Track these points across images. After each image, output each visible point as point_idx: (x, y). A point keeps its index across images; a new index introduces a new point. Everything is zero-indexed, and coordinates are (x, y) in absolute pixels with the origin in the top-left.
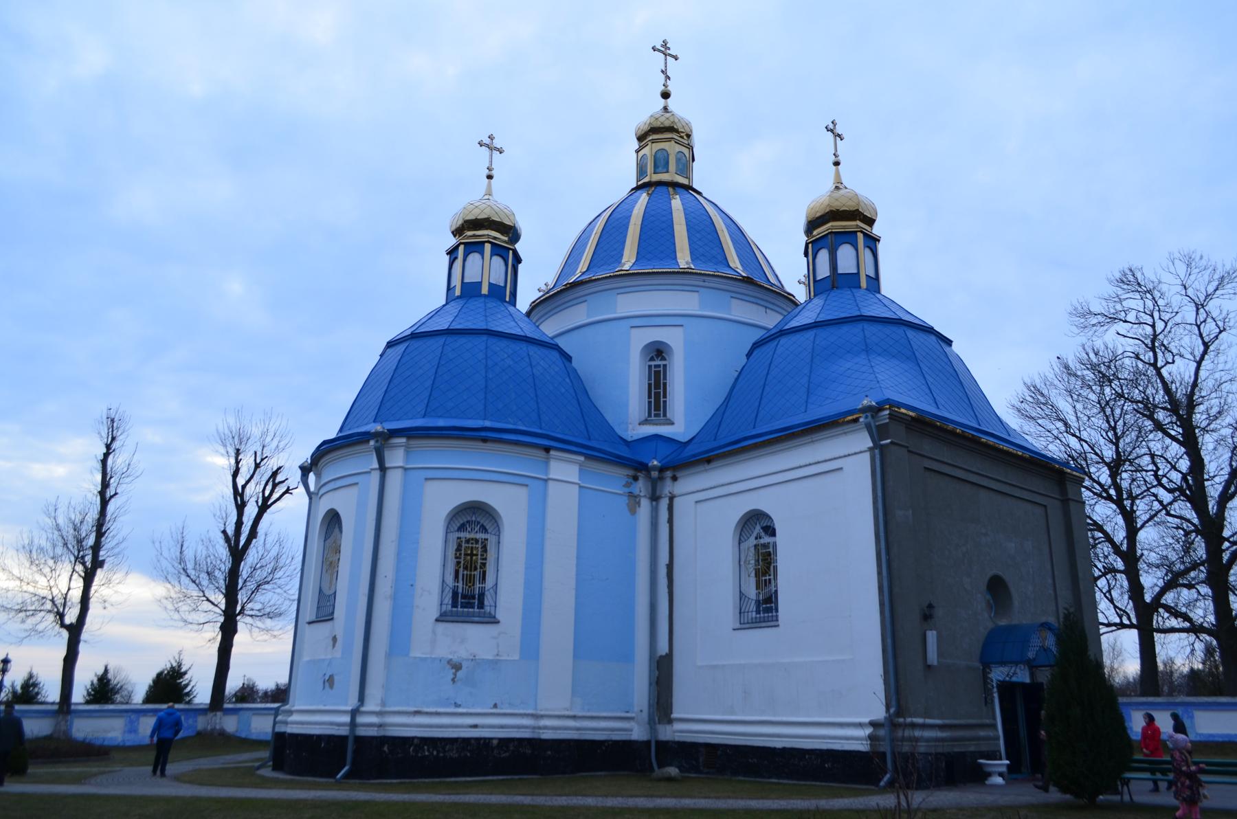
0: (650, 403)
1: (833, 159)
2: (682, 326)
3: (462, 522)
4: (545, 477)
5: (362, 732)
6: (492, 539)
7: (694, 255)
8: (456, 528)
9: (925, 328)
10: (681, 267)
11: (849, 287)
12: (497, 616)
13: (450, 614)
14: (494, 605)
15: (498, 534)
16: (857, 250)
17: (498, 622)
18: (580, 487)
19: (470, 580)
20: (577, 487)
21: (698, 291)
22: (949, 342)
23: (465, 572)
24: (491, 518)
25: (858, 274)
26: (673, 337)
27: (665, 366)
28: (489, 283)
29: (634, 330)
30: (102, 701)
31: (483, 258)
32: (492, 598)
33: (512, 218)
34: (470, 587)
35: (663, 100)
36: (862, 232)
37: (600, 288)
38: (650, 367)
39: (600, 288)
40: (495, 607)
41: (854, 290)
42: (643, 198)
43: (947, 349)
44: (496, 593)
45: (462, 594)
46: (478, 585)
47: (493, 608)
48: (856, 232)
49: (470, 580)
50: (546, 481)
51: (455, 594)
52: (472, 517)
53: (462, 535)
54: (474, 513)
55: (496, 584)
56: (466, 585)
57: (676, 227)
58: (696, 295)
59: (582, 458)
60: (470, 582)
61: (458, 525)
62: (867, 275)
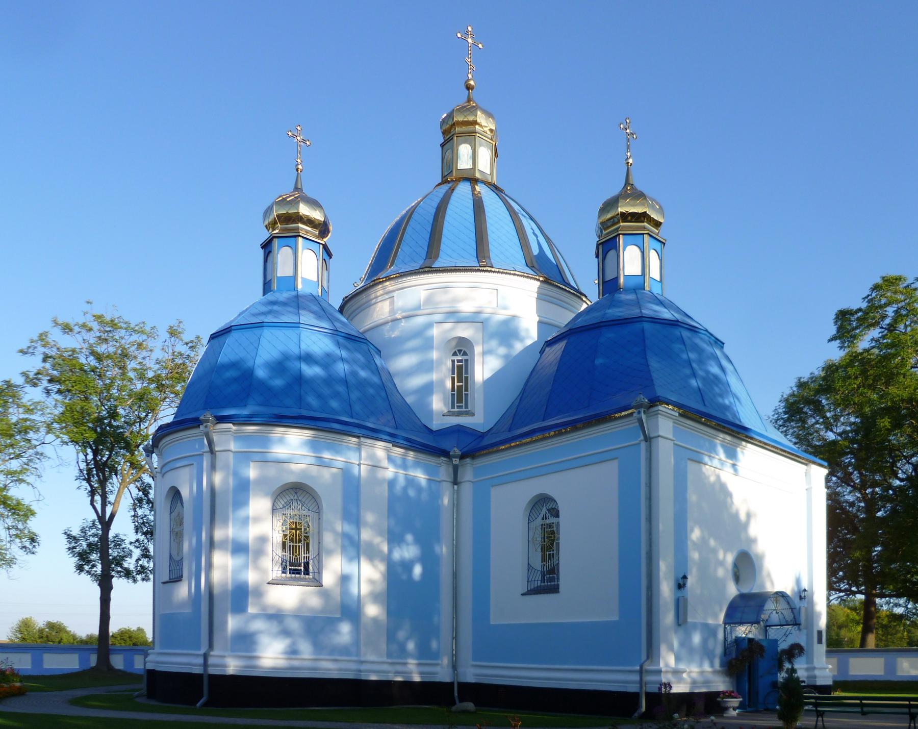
38: (453, 361)
56: (293, 554)
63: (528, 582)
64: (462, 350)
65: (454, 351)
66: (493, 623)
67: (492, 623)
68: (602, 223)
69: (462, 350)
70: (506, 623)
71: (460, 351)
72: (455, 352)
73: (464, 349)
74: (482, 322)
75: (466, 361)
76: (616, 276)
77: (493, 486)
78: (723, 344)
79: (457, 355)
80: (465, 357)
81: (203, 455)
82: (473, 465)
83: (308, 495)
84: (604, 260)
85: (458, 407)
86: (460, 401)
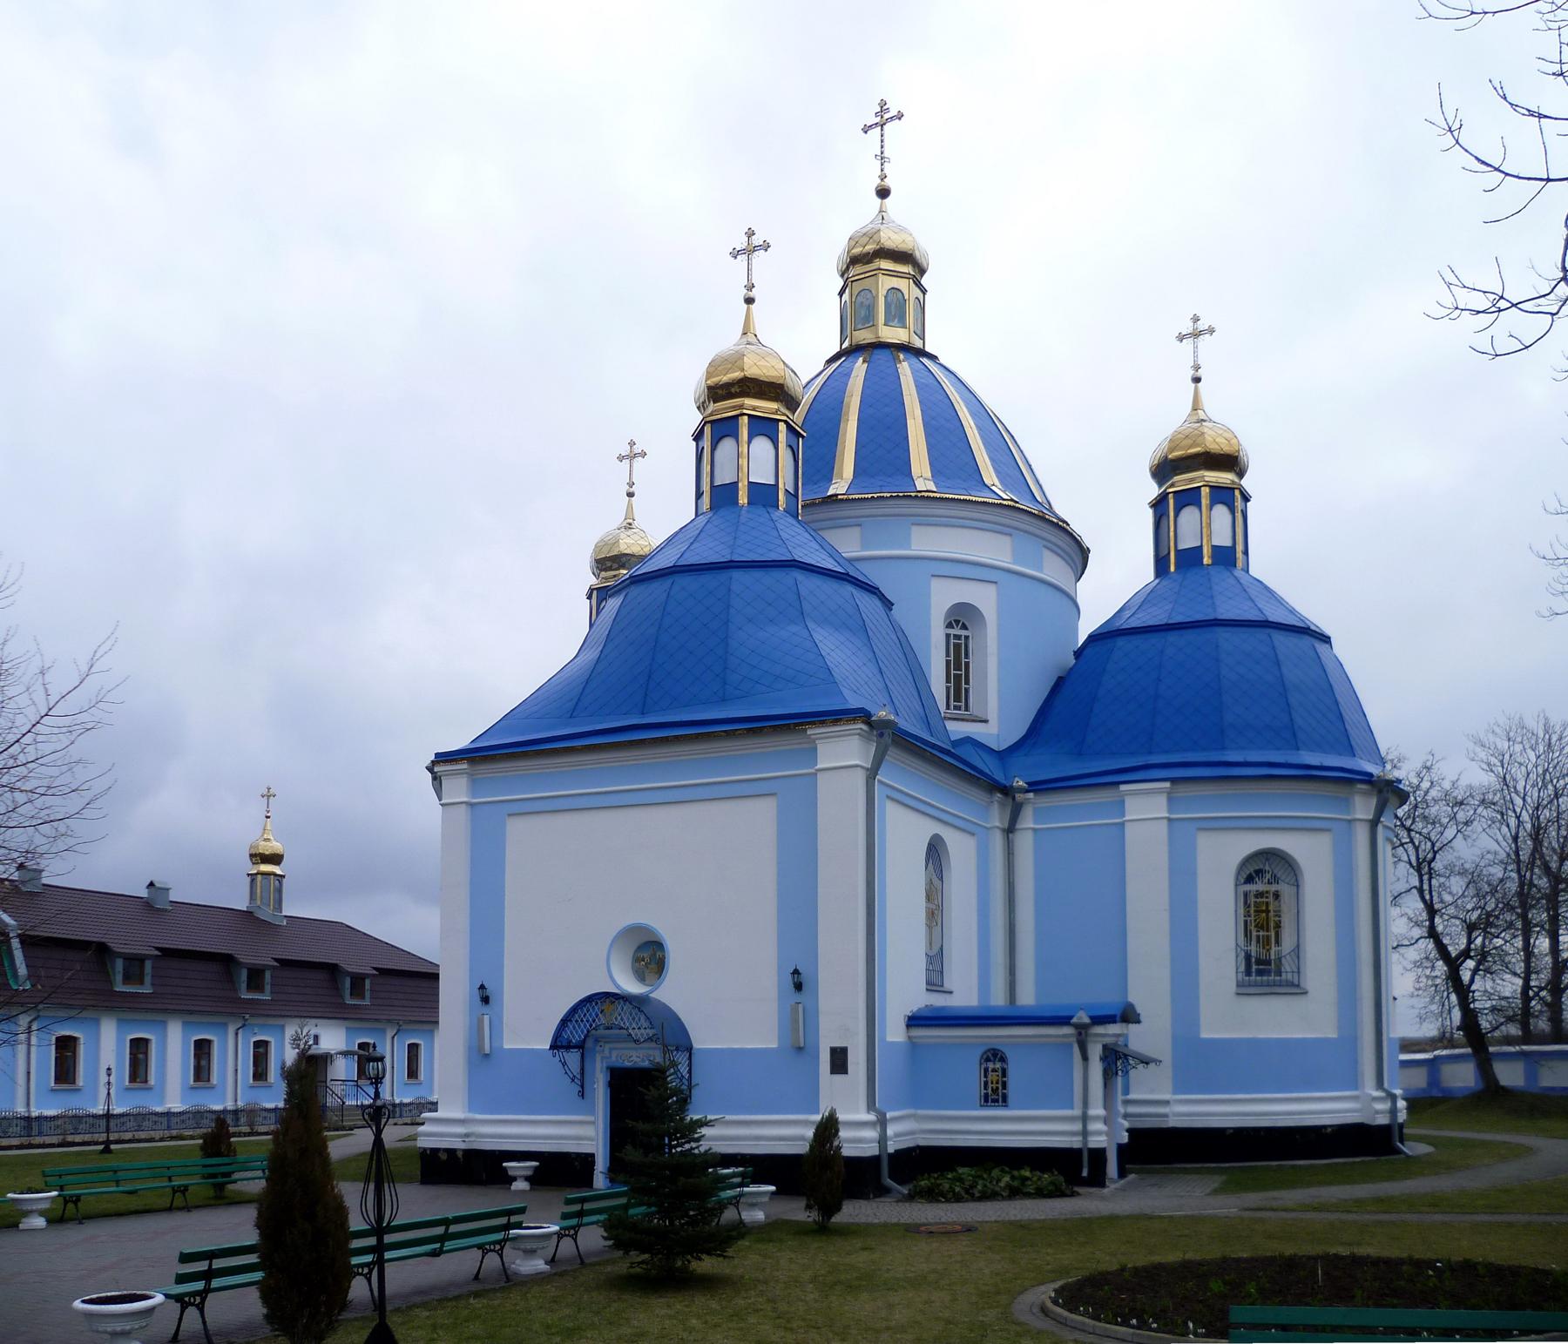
0: (948, 689)
1: (1191, 372)
2: (996, 583)
3: (1248, 873)
4: (1349, 818)
5: (1092, 1145)
6: (1285, 889)
7: (937, 472)
8: (1242, 881)
9: (839, 575)
10: (918, 489)
11: (764, 506)
12: (1302, 985)
13: (1284, 984)
14: (1296, 970)
15: (1297, 885)
16: (776, 448)
17: (1306, 993)
18: (1169, 820)
19: (1265, 943)
20: (1165, 821)
21: (1010, 535)
22: (1326, 639)
23: (1261, 933)
24: (1287, 866)
25: (776, 485)
26: (984, 598)
27: (967, 638)
28: (749, 482)
29: (933, 578)
30: (1329, 1130)
31: (738, 442)
32: (1293, 961)
33: (1234, 441)
34: (1268, 950)
35: (879, 200)
36: (785, 422)
37: (897, 511)
38: (948, 636)
39: (897, 511)
40: (1299, 972)
41: (770, 510)
42: (860, 367)
43: (1321, 648)
44: (1298, 957)
45: (1256, 958)
46: (1274, 949)
47: (1296, 975)
48: (1234, 488)
49: (1265, 943)
50: (1350, 821)
51: (1248, 957)
52: (1265, 865)
53: (1248, 887)
54: (1267, 859)
55: (1298, 946)
56: (1264, 948)
57: (910, 422)
58: (1007, 540)
59: (1167, 785)
60: (1268, 945)
61: (1245, 876)
62: (786, 490)
63: (1237, 972)
64: (959, 621)
65: (948, 621)
66: (891, 1040)
67: (1204, 1035)
68: (710, 388)
69: (959, 621)
70: (1300, 1036)
71: (957, 622)
72: (951, 622)
73: (962, 620)
74: (996, 583)
75: (967, 638)
76: (1199, 544)
77: (509, 815)
78: (893, 605)
79: (953, 628)
80: (963, 633)
81: (816, 774)
82: (472, 775)
83: (1283, 861)
84: (714, 449)
85: (956, 708)
86: (958, 699)
